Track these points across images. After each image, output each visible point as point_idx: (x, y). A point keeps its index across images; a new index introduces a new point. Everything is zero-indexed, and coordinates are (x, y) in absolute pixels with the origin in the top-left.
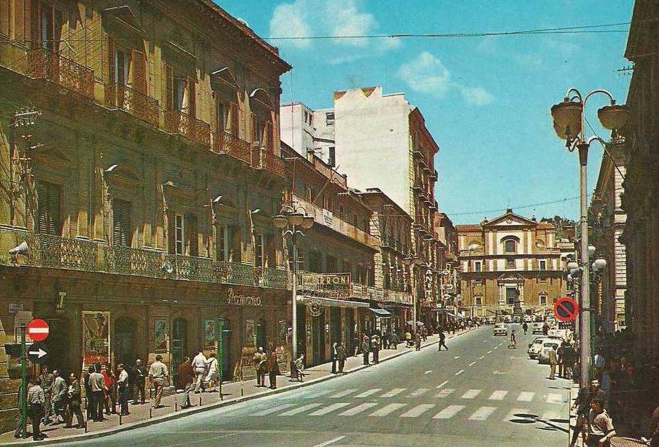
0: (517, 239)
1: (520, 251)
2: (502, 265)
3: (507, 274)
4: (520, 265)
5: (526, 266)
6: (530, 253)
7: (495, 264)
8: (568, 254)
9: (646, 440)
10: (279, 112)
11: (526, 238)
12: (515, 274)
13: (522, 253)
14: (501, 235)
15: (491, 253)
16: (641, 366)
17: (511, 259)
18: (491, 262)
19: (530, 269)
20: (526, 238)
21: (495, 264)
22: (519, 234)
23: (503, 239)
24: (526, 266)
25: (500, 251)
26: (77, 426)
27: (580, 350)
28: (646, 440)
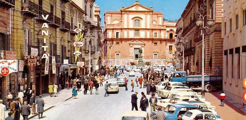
0: (141, 19)
1: (143, 27)
2: (132, 34)
4: (142, 34)
5: (146, 36)
7: (128, 33)
11: (146, 19)
12: (140, 39)
13: (144, 28)
14: (132, 16)
21: (128, 33)
22: (142, 16)
23: (133, 19)
24: (146, 36)
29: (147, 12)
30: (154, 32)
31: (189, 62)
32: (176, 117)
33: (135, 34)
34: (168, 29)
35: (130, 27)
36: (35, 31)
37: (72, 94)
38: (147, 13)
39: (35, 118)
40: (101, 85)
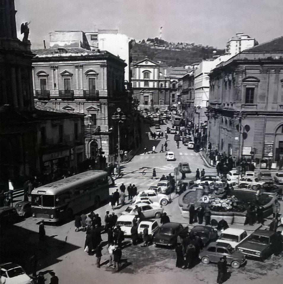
0: (150, 72)
1: (151, 78)
2: (142, 85)
3: (144, 89)
4: (151, 85)
5: (154, 86)
6: (156, 79)
7: (139, 84)
8: (173, 80)
9: (165, 73)
10: (86, 39)
11: (154, 72)
12: (150, 89)
13: (153, 79)
14: (142, 70)
15: (137, 78)
16: (177, 132)
17: (146, 82)
18: (137, 83)
19: (156, 87)
20: (154, 72)
21: (139, 84)
22: (151, 70)
23: (143, 72)
24: (154, 86)
25: (142, 78)
26: (34, 217)
27: (139, 193)
28: (165, 73)
29: (155, 66)
30: (160, 83)
31: (265, 125)
32: (102, 127)
33: (145, 85)
34: (172, 80)
35: (141, 79)
36: (174, 89)
37: (280, 268)
38: (154, 67)
39: (80, 175)
40: (105, 123)
